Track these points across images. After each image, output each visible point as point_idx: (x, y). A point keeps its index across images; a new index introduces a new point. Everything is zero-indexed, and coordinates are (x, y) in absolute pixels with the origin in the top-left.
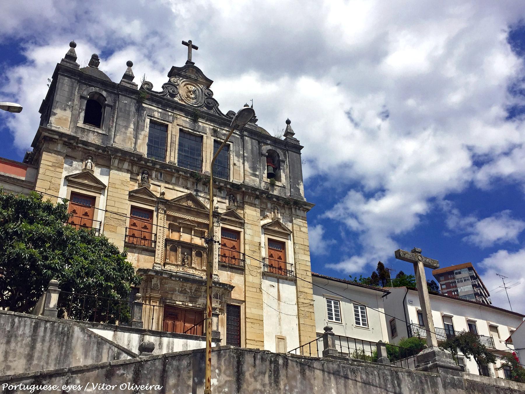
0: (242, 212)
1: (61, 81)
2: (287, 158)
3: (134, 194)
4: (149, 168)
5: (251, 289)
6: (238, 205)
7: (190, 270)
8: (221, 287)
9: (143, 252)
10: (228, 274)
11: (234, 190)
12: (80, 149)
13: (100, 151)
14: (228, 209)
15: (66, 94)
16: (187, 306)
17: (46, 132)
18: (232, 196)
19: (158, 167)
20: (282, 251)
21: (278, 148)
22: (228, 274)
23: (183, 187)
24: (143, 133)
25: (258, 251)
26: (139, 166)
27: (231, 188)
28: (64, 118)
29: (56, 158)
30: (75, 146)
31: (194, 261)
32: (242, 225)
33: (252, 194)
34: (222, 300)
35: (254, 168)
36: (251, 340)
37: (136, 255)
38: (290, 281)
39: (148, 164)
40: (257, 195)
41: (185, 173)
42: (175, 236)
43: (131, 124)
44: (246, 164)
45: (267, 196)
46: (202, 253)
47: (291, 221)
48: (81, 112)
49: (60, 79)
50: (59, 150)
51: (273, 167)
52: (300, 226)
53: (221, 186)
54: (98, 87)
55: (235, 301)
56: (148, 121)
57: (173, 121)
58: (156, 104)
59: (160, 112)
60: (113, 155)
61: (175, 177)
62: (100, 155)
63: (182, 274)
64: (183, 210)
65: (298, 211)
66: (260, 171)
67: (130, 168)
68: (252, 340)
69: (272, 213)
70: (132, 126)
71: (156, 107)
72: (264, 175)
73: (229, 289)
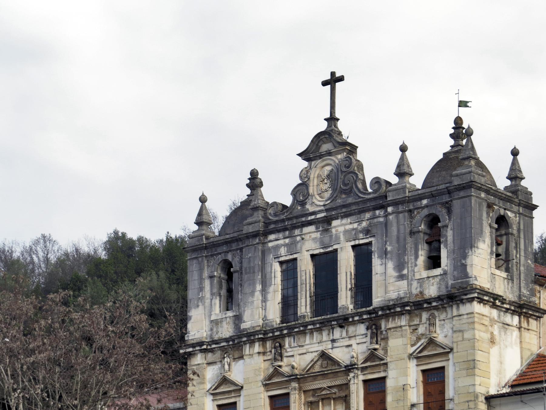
26: (271, 340)
61: (309, 334)
64: (319, 377)
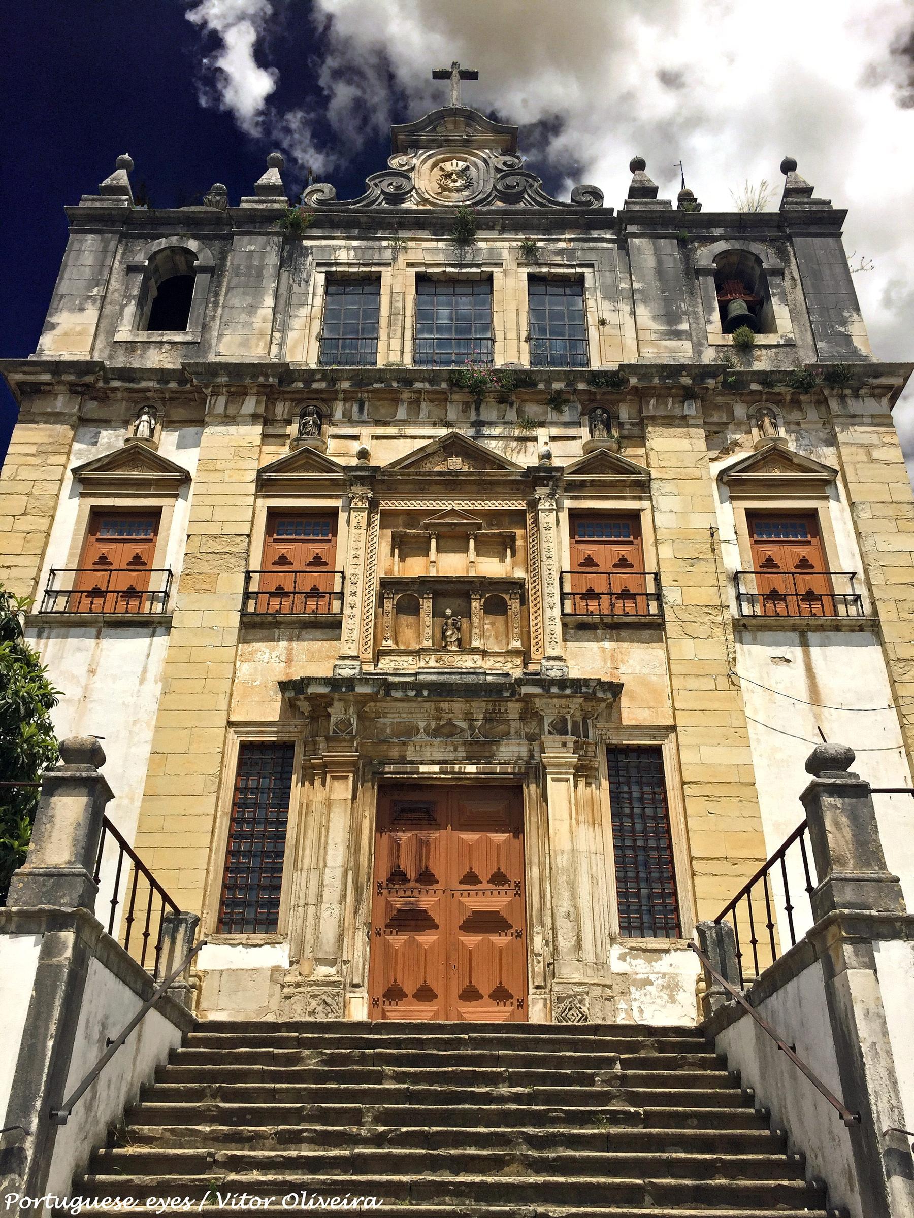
0: (641, 451)
1: (76, 246)
2: (793, 259)
3: (274, 476)
4: (323, 396)
5: (693, 683)
6: (626, 433)
7: (464, 658)
8: (568, 691)
9: (304, 632)
10: (603, 650)
11: (604, 394)
12: (119, 395)
13: (173, 385)
14: (587, 449)
15: (87, 273)
16: (460, 773)
17: (16, 373)
18: (599, 411)
19: (345, 385)
20: (809, 543)
21: (755, 239)
22: (603, 650)
23: (434, 424)
24: (304, 311)
25: (710, 555)
26: (292, 400)
27: (593, 389)
28: (78, 329)
29: (48, 433)
30: (105, 390)
31: (477, 631)
32: (643, 487)
33: (670, 388)
34: (586, 736)
35: (670, 317)
36: (712, 859)
37: (284, 644)
38: (853, 631)
39: (315, 386)
40: (685, 387)
41: (431, 382)
42: (415, 567)
43: (265, 298)
44: (641, 310)
45: (724, 383)
46: (507, 599)
47: (832, 441)
48: (127, 305)
49: (72, 242)
50: (58, 410)
51: (746, 302)
52: (867, 448)
53: (559, 392)
54: (177, 235)
55: (636, 732)
56: (321, 279)
57: (394, 259)
58: (344, 231)
59: (355, 248)
60: (207, 387)
61: (406, 404)
62: (177, 395)
63: (434, 677)
64: (434, 488)
65: (851, 402)
66: (696, 318)
67: (261, 410)
68: (718, 859)
69: (755, 431)
70: (269, 301)
71: (343, 238)
72: (709, 328)
73: (600, 695)
